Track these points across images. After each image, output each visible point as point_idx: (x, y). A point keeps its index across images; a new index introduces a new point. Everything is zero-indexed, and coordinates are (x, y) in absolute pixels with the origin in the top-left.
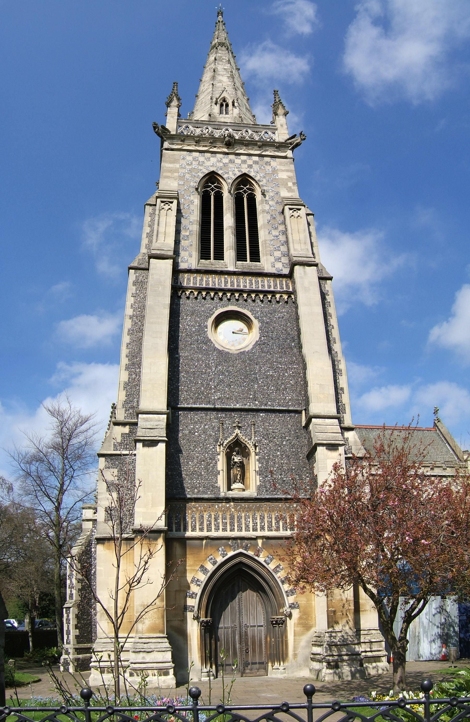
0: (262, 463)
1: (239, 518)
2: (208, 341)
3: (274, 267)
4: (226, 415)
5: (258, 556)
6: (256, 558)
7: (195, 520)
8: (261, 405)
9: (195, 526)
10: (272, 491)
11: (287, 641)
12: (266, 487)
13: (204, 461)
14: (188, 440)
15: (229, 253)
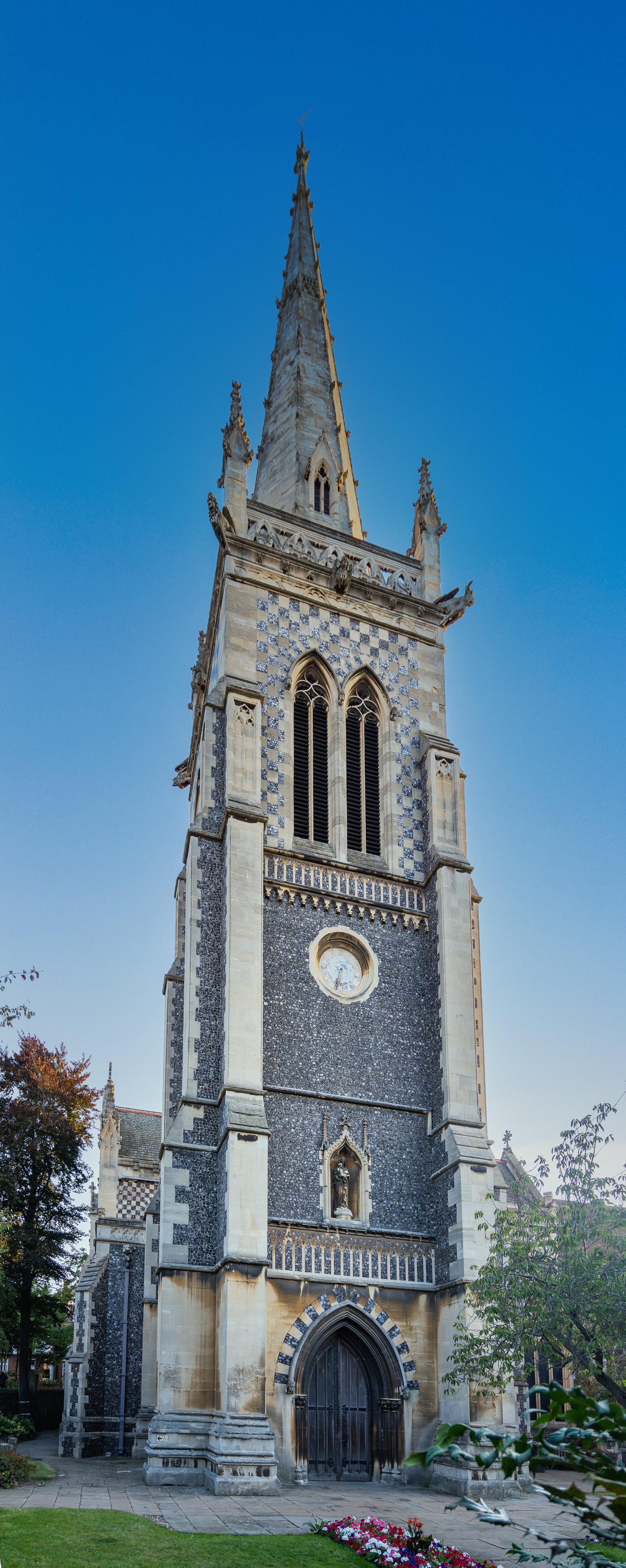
0: (376, 1182)
1: (347, 1256)
2: (309, 979)
3: (403, 867)
4: (331, 1107)
5: (370, 1311)
6: (367, 1313)
7: (290, 1254)
8: (376, 1098)
9: (291, 1262)
10: (387, 1223)
11: (403, 1434)
12: (380, 1216)
13: (302, 1171)
14: (282, 1138)
15: (338, 832)
